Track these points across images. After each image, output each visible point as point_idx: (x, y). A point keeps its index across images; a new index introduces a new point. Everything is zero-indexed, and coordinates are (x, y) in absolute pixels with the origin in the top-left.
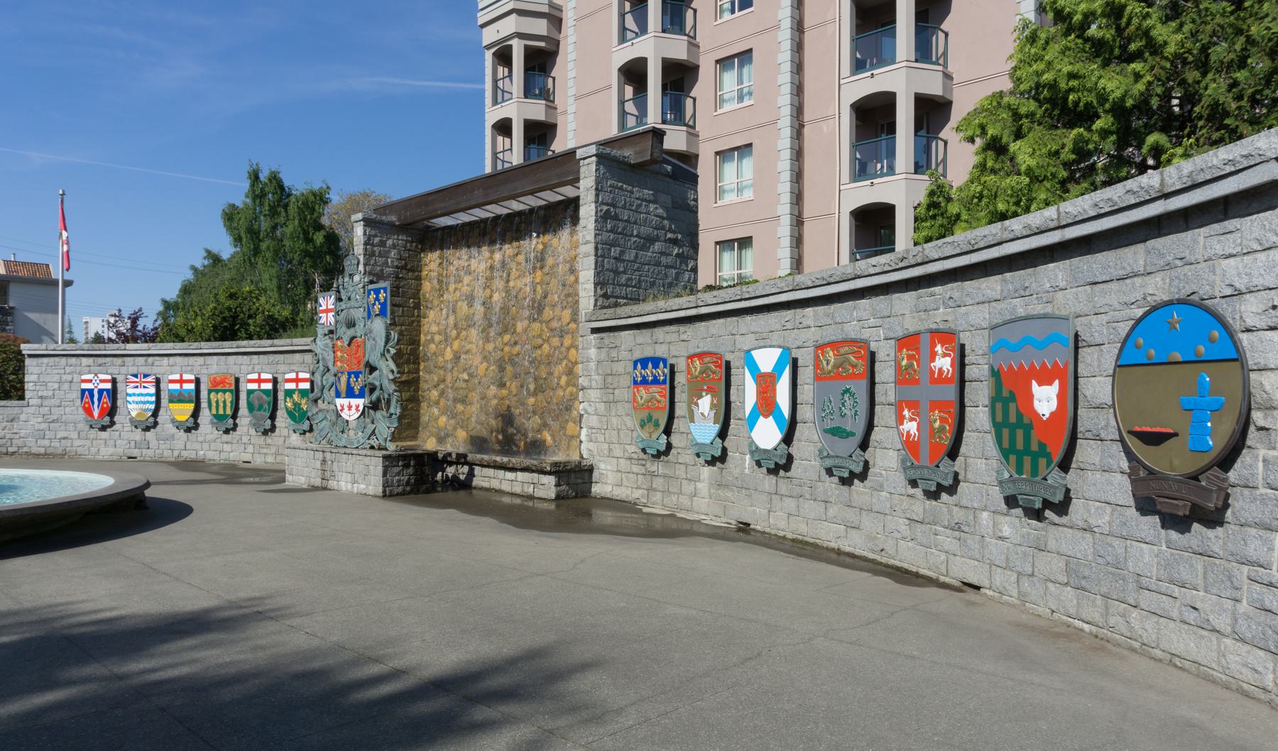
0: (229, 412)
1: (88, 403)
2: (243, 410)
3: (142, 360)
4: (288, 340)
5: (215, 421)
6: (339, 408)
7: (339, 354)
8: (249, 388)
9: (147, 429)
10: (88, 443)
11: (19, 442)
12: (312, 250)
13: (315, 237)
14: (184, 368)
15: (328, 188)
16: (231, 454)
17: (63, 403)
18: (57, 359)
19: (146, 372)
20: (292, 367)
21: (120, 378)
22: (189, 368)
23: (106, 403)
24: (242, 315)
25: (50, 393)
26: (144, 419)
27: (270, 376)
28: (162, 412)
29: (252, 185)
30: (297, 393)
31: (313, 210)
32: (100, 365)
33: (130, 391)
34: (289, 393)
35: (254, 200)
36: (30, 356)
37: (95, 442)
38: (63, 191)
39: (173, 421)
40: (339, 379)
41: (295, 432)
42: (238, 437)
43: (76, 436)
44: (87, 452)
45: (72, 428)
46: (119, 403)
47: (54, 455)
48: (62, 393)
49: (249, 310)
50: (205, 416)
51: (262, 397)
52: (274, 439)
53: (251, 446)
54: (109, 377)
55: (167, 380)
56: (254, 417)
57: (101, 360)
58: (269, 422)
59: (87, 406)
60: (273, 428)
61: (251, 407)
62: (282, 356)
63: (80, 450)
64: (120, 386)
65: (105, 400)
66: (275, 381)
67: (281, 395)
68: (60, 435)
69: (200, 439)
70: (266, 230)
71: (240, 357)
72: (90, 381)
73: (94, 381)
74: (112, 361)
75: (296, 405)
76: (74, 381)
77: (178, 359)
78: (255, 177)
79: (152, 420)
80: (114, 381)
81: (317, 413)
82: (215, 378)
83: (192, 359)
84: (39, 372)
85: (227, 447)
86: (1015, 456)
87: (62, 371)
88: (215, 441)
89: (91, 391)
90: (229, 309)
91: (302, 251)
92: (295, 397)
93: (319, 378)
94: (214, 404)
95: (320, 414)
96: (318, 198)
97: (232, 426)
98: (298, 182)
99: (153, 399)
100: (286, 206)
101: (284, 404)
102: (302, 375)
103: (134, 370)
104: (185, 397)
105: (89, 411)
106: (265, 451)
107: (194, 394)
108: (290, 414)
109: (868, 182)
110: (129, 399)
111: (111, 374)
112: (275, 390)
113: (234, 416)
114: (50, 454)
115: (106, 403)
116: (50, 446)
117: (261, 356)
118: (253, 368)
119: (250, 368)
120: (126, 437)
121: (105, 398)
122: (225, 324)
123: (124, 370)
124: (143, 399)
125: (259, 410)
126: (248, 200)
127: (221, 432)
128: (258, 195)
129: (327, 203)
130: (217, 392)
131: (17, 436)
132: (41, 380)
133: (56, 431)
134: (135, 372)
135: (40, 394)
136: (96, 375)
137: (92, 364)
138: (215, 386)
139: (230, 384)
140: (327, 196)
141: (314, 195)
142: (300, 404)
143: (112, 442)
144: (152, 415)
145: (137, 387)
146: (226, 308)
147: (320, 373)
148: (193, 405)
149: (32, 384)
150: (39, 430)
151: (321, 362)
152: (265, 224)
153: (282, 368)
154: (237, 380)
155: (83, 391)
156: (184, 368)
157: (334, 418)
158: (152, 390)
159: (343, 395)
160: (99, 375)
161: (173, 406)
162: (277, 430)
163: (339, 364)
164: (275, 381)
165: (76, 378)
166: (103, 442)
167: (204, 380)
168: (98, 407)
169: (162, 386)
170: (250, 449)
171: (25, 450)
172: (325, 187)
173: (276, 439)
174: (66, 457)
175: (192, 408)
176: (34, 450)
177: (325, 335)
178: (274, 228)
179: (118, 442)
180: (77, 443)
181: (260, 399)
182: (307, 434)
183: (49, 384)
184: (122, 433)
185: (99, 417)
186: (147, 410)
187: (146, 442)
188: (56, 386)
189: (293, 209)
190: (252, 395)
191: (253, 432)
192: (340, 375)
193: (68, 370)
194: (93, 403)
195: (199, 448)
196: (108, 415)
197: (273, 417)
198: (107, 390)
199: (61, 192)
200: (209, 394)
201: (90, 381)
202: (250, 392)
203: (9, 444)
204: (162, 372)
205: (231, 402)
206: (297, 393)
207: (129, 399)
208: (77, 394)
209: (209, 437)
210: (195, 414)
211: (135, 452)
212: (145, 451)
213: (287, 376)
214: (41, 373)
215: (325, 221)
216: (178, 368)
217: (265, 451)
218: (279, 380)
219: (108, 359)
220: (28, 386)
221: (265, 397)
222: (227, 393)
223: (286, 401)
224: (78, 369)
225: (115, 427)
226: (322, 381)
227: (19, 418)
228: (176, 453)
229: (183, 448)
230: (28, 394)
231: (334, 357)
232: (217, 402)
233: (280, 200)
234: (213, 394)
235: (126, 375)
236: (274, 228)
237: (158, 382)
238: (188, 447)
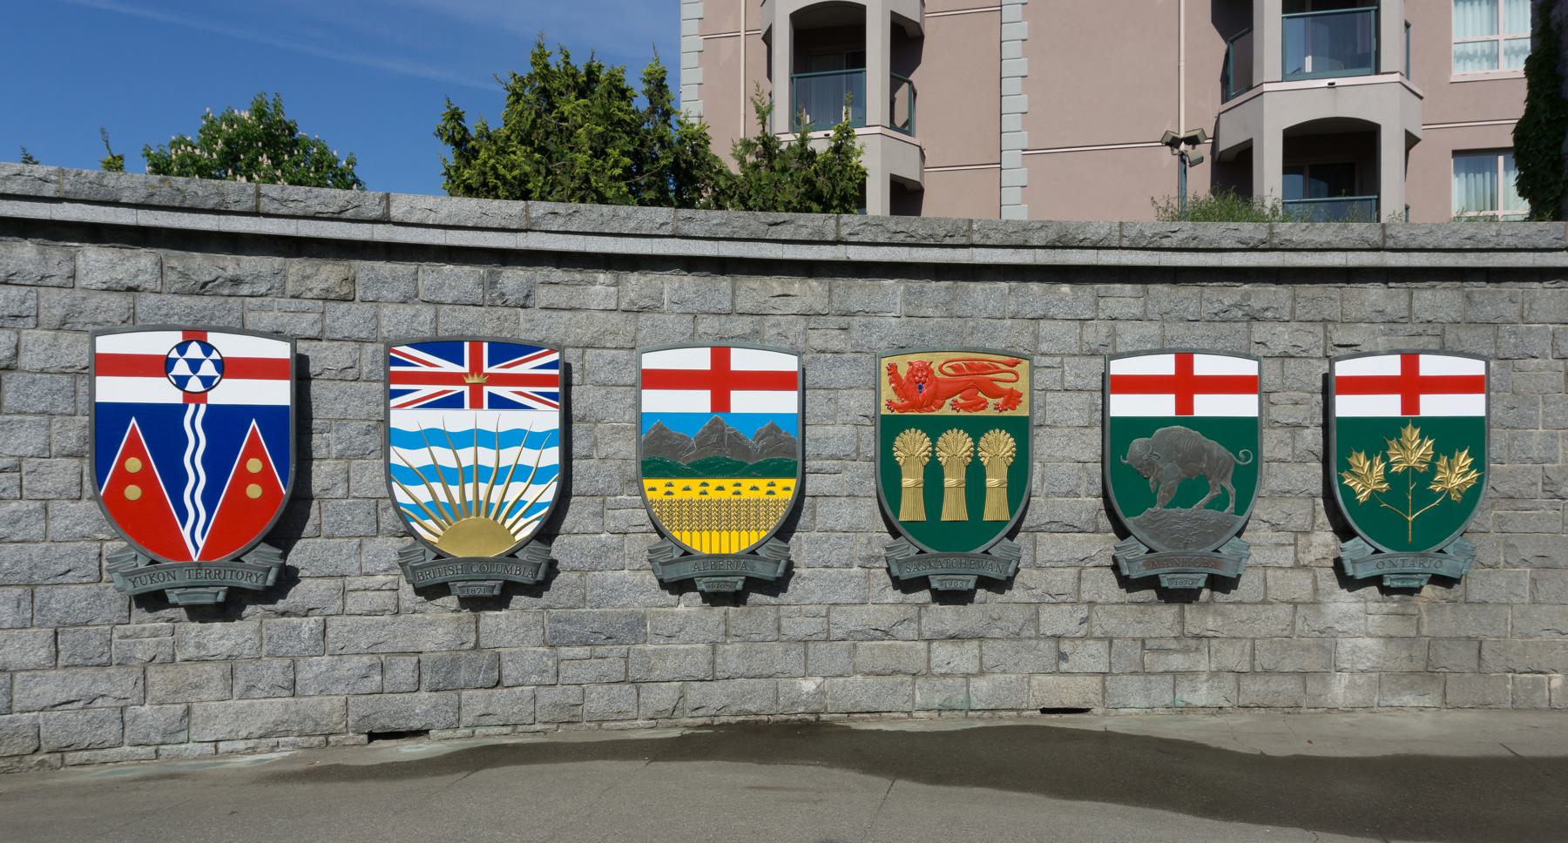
1: (143, 478)
8: (645, 366)
10: (121, 683)
21: (323, 357)
32: (202, 289)
44: (111, 732)
54: (279, 350)
57: (202, 265)
69: (800, 626)
71: (1035, 287)
73: (181, 368)
76: (25, 361)
77: (671, 284)
85: (963, 657)
86: (707, 367)
99: (552, 456)
104: (746, 451)
106: (1177, 662)
109: (1325, 83)
111: (293, 340)
115: (264, 478)
117: (1159, 290)
121: (134, 449)
123: (346, 318)
130: (935, 428)
136: (194, 334)
137: (146, 280)
145: (455, 402)
155: (110, 419)
165: (73, 351)
166: (215, 671)
168: (210, 498)
173: (1242, 613)
179: (313, 669)
184: (334, 623)
190: (1137, 444)
194: (177, 480)
198: (267, 415)
207: (401, 456)
208: (76, 431)
209: (847, 620)
212: (476, 701)
217: (1177, 662)
219: (249, 264)
224: (54, 303)
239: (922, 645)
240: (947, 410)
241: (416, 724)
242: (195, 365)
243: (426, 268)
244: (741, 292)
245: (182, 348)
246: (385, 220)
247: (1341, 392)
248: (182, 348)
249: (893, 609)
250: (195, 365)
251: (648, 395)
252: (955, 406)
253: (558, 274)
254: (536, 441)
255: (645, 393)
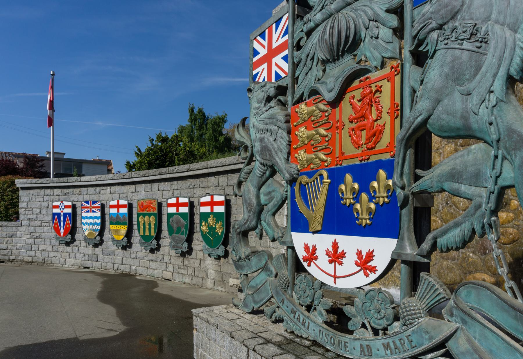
0: (153, 234)
2: (165, 233)
3: (92, 189)
4: (203, 163)
5: (143, 241)
6: (301, 253)
7: (303, 132)
9: (96, 246)
10: (58, 255)
11: (15, 252)
12: (218, 145)
13: (220, 139)
14: (121, 195)
15: (226, 115)
16: (156, 271)
17: (43, 224)
18: (38, 190)
19: (95, 199)
20: (208, 191)
21: (78, 204)
22: (125, 195)
23: (69, 224)
24: (170, 154)
25: (35, 216)
26: (93, 238)
27: (186, 200)
28: (106, 232)
29: (191, 115)
30: (212, 216)
31: (219, 126)
32: (65, 194)
33: (84, 215)
34: (204, 217)
35: (191, 122)
36: (23, 189)
37: (63, 254)
38: (53, 72)
39: (113, 240)
40: (302, 187)
41: (210, 256)
42: (161, 257)
43: (51, 249)
45: (48, 243)
46: (78, 224)
47: (38, 263)
48: (42, 216)
49: (176, 151)
50: (136, 238)
51: (180, 221)
52: (192, 261)
53: (171, 266)
54: (70, 204)
55: (108, 206)
56: (173, 239)
57: (66, 191)
58: (186, 245)
59: (56, 226)
60: (190, 251)
61: (171, 231)
62: (198, 180)
63: (54, 260)
64: (78, 210)
65: (68, 222)
66: (191, 205)
67: (197, 219)
68: (42, 248)
69: (133, 256)
70: (197, 136)
72: (57, 207)
73: (60, 207)
74: (73, 191)
75: (212, 229)
77: (117, 188)
78: (192, 111)
79: (98, 238)
80: (74, 207)
81: (248, 257)
82: (142, 203)
83: (127, 188)
84: (28, 200)
85: (152, 265)
87: (42, 200)
88: (143, 259)
89: (59, 215)
90: (161, 149)
91: (214, 146)
92: (210, 220)
93: (253, 190)
94: (142, 226)
95: (254, 260)
96: (221, 120)
97: (155, 246)
98: (212, 113)
99: (99, 221)
100: (206, 125)
101: (201, 228)
102: (217, 198)
103: (87, 198)
105: (57, 230)
106: (182, 271)
107: (127, 217)
108: (205, 237)
110: (84, 221)
112: (192, 213)
113: (158, 237)
114: (35, 262)
116: (35, 256)
118: (173, 193)
119: (171, 192)
120: (82, 252)
122: (158, 162)
123: (81, 198)
124: (92, 221)
125: (177, 233)
126: (189, 123)
127: (148, 251)
128: (193, 120)
129: (225, 122)
130: (144, 215)
131: (15, 248)
132: (29, 206)
133: (38, 245)
134: (88, 199)
135: (29, 216)
136: (62, 202)
137: (60, 194)
138: (143, 211)
139: (154, 208)
140: (226, 119)
141: (219, 118)
142: (215, 228)
143: (73, 255)
144: (99, 235)
145: (88, 212)
146: (159, 149)
147: (255, 182)
148: (126, 226)
149: (23, 210)
150: (28, 244)
151: (258, 157)
152: (197, 133)
153: (198, 192)
154: (160, 205)
155: (54, 214)
156: (121, 195)
157: (286, 273)
158: (98, 214)
159: (316, 224)
160: (64, 202)
161: (113, 227)
162: (194, 252)
163: (302, 154)
164: (191, 205)
166: (67, 254)
167: (135, 205)
169: (106, 210)
170: (171, 268)
171: (20, 258)
172: (224, 114)
173: (192, 261)
174: (45, 264)
175: (126, 229)
176: (26, 259)
177: (269, 99)
178: (201, 136)
179: (78, 255)
180: (52, 254)
181: (178, 222)
182: (222, 259)
183: (34, 210)
184: (80, 248)
185: (64, 235)
186: (95, 230)
187: (95, 256)
188: (38, 211)
189: (209, 126)
190: (171, 219)
191: (173, 253)
192: (304, 179)
193: (46, 198)
195: (131, 263)
196: (70, 234)
197: (189, 240)
199: (52, 73)
200: (138, 217)
201: (57, 207)
202: (170, 215)
203: (10, 253)
204: (106, 198)
205: (155, 224)
206: (212, 216)
207: (84, 221)
208: (50, 218)
210: (129, 235)
211: (88, 264)
213: (203, 200)
214: (29, 201)
215: (224, 132)
216: (117, 196)
217: (182, 271)
218: (196, 203)
219: (71, 190)
220: (21, 211)
221: (182, 220)
222: (152, 217)
223: (201, 225)
225: (75, 243)
226: (258, 197)
227: (16, 234)
228: (116, 266)
229: (120, 262)
230: (21, 217)
231: (290, 143)
232: (144, 224)
233: (203, 122)
234: (141, 217)
235: (82, 202)
236: (201, 136)
237: (103, 208)
238: (124, 262)
239: (148, 262)
240: (146, 212)
241: (88, 266)
242: (62, 206)
243: (112, 188)
244: (112, 189)
245: (60, 204)
246: (80, 181)
247: (126, 205)
248: (60, 204)
249: (144, 253)
250: (62, 206)
251: (111, 209)
252: (147, 211)
253: (103, 188)
254: (96, 218)
255: (110, 209)
